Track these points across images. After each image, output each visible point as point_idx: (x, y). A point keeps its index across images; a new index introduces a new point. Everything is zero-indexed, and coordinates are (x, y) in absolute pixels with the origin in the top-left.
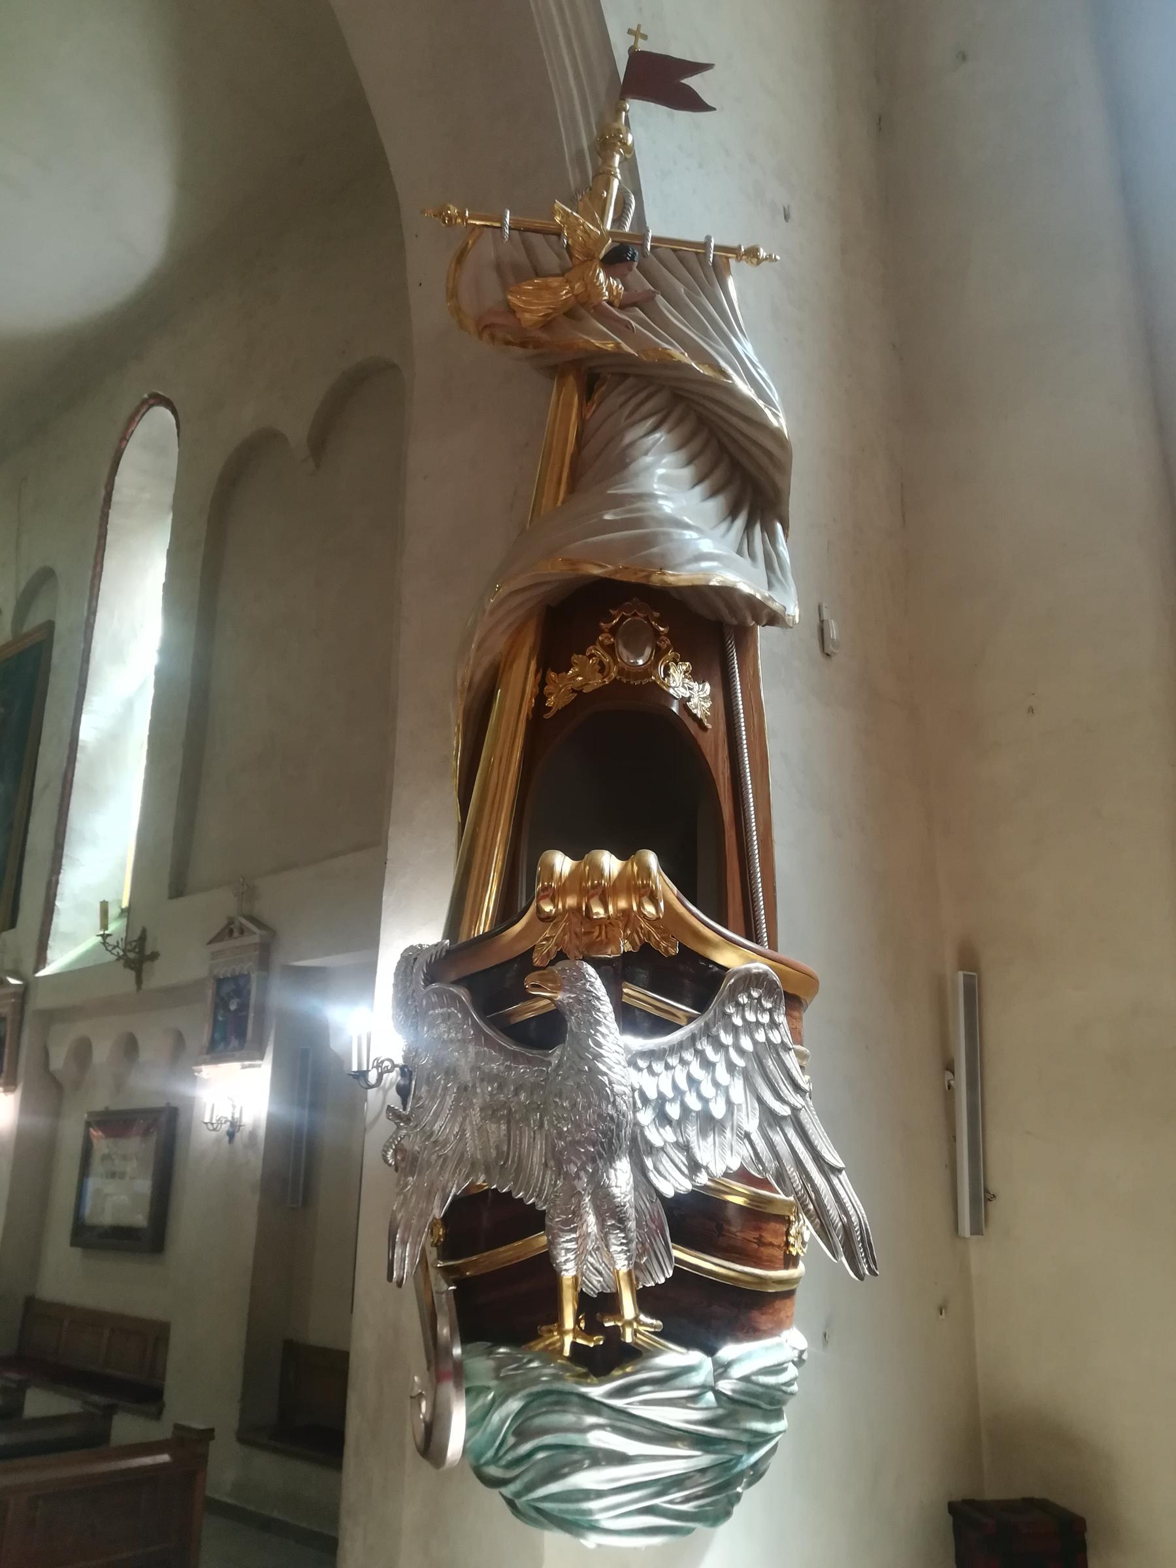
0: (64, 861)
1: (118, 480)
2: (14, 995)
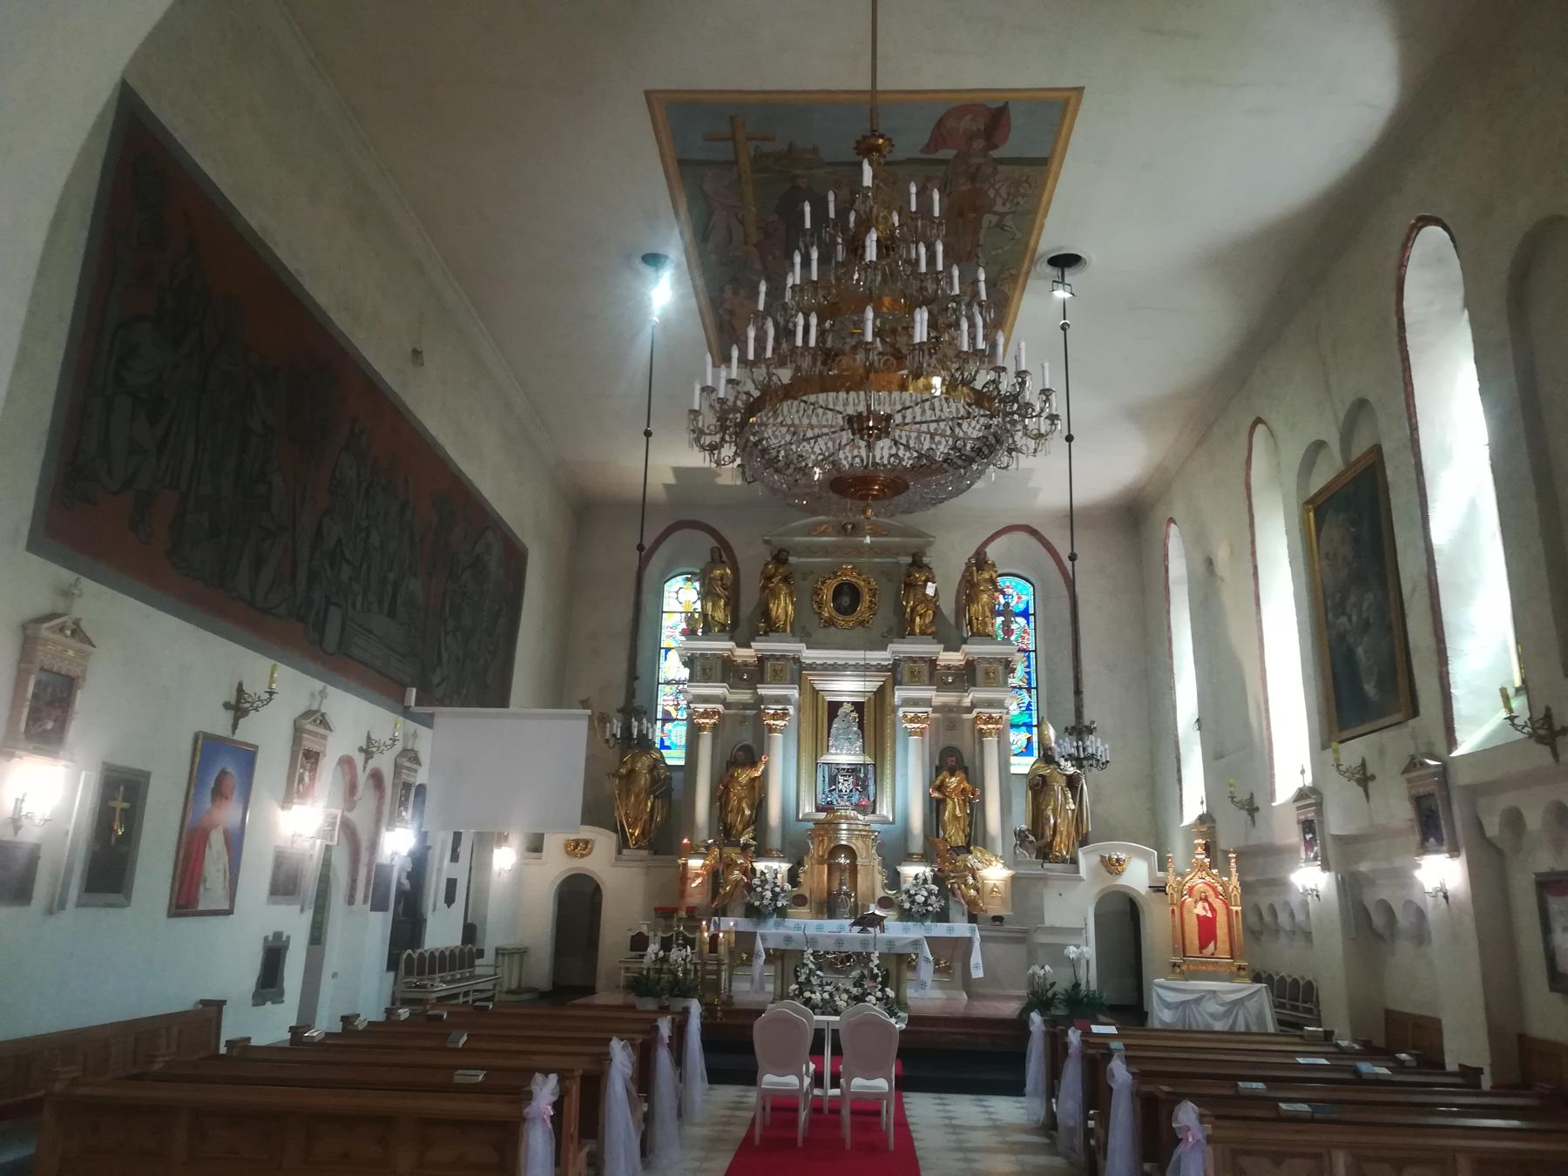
0: (1449, 653)
1: (1406, 304)
2: (1434, 775)
